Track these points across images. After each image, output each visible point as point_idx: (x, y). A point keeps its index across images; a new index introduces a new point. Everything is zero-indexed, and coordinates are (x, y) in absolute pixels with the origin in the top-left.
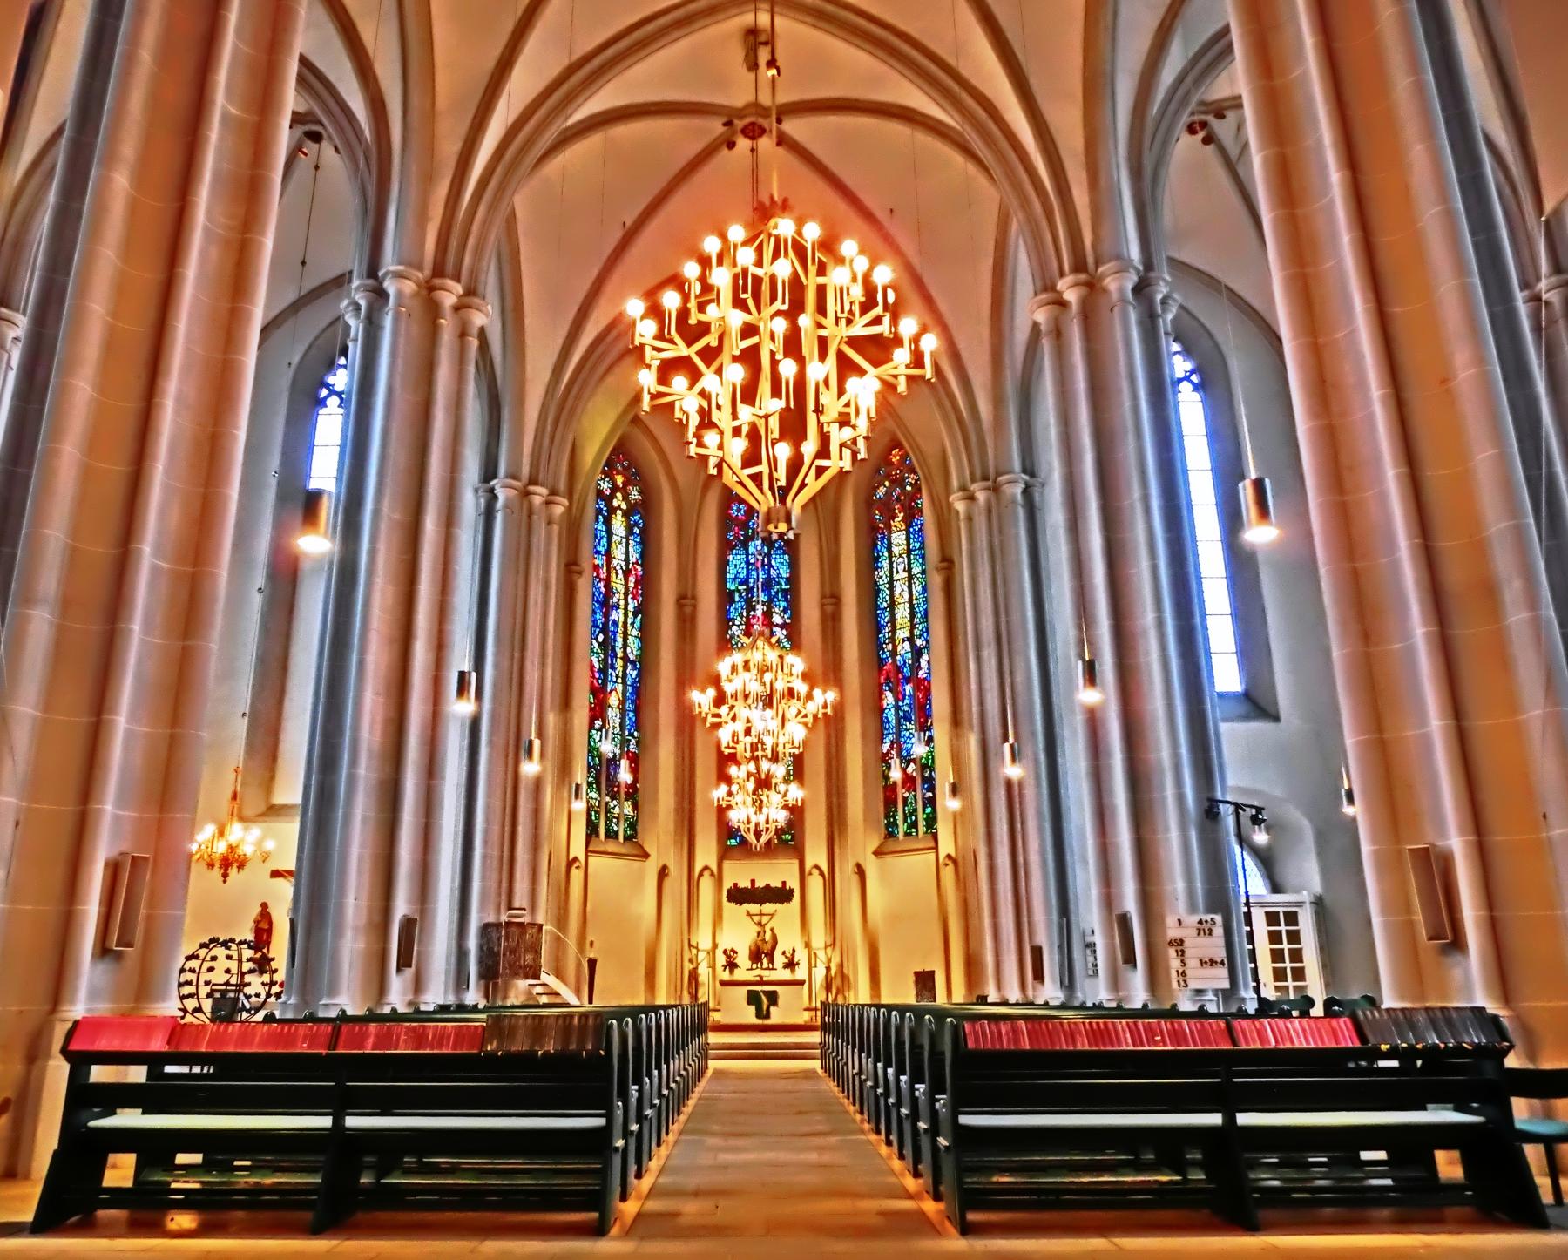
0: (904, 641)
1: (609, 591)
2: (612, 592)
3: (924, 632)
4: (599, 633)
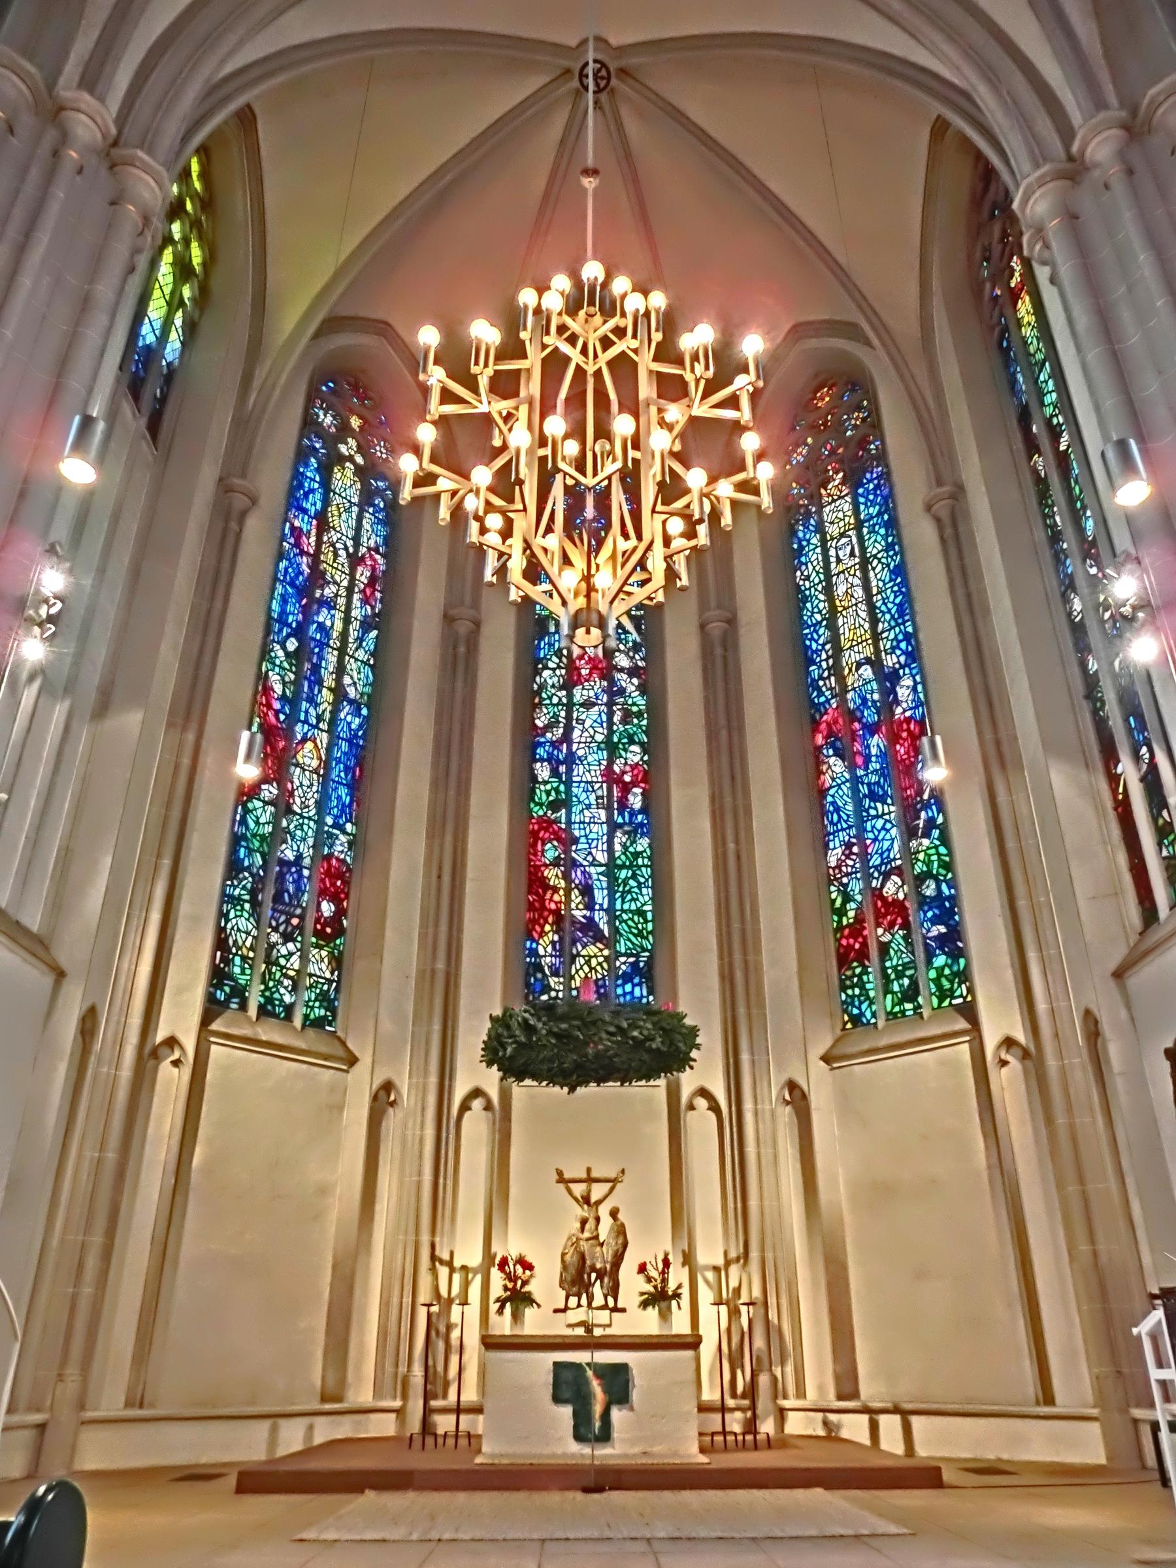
0: (859, 665)
1: (318, 576)
2: (324, 579)
3: (899, 642)
4: (288, 636)
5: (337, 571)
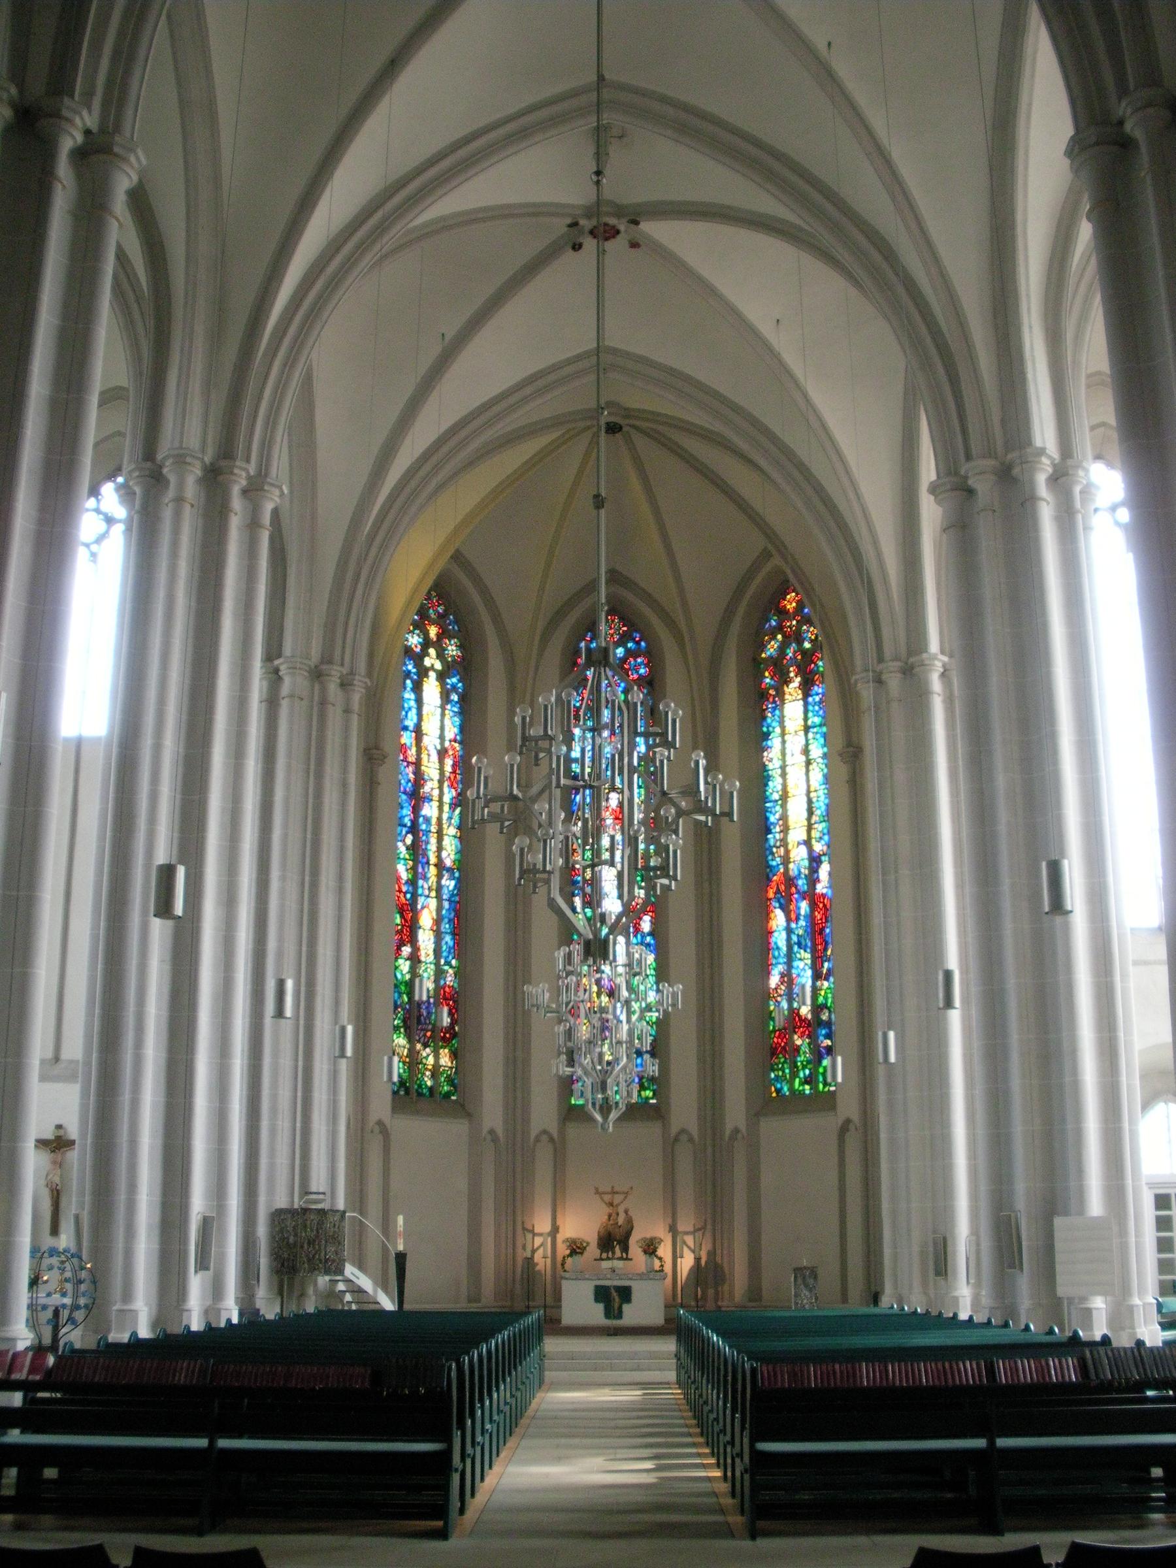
5: (431, 768)
